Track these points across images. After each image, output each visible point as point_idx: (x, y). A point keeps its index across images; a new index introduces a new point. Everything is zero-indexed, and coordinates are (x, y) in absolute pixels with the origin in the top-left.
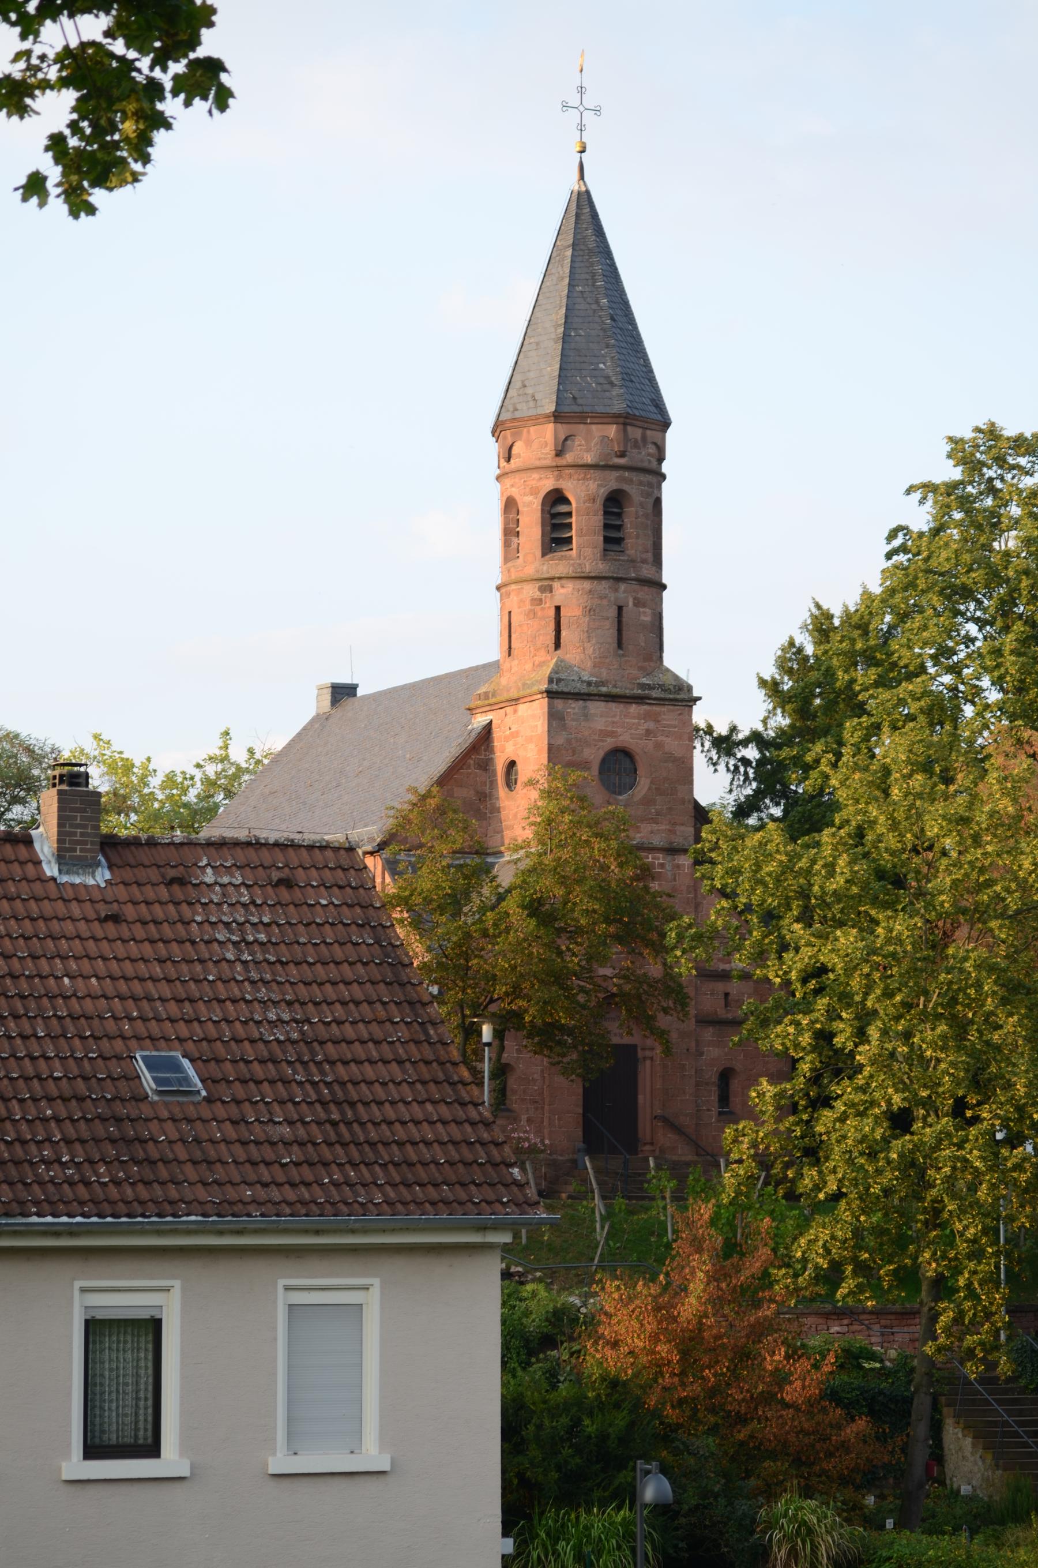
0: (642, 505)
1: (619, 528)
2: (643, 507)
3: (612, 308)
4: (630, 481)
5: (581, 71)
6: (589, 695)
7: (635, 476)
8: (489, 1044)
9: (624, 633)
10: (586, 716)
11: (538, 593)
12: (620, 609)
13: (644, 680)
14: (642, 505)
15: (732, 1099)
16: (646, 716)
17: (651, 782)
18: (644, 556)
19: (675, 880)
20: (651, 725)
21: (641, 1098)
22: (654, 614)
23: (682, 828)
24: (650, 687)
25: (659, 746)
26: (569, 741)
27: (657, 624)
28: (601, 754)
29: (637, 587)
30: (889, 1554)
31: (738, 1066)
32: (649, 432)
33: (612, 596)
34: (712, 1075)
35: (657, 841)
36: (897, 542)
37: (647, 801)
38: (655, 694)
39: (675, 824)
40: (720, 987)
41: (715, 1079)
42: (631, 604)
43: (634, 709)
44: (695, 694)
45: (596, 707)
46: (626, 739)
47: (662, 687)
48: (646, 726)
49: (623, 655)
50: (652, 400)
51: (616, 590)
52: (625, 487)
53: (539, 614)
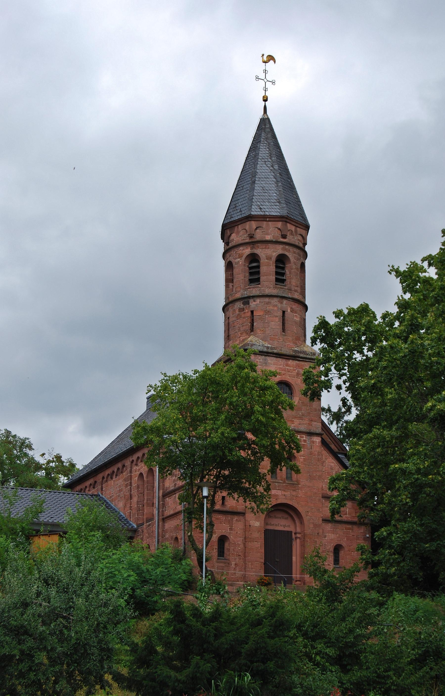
1: (283, 274)
2: (295, 265)
3: (280, 170)
6: (268, 353)
7: (291, 249)
8: (206, 497)
9: (286, 325)
11: (242, 305)
12: (284, 312)
15: (340, 561)
16: (298, 366)
17: (299, 399)
18: (296, 288)
19: (312, 449)
21: (294, 558)
22: (301, 318)
23: (315, 423)
24: (298, 352)
27: (303, 323)
29: (293, 303)
31: (344, 544)
32: (298, 229)
33: (279, 305)
35: (302, 428)
38: (302, 355)
39: (312, 420)
41: (332, 549)
42: (289, 311)
43: (290, 362)
45: (271, 360)
47: (304, 353)
49: (285, 335)
50: (300, 214)
51: (282, 303)
52: (287, 253)
53: (243, 316)
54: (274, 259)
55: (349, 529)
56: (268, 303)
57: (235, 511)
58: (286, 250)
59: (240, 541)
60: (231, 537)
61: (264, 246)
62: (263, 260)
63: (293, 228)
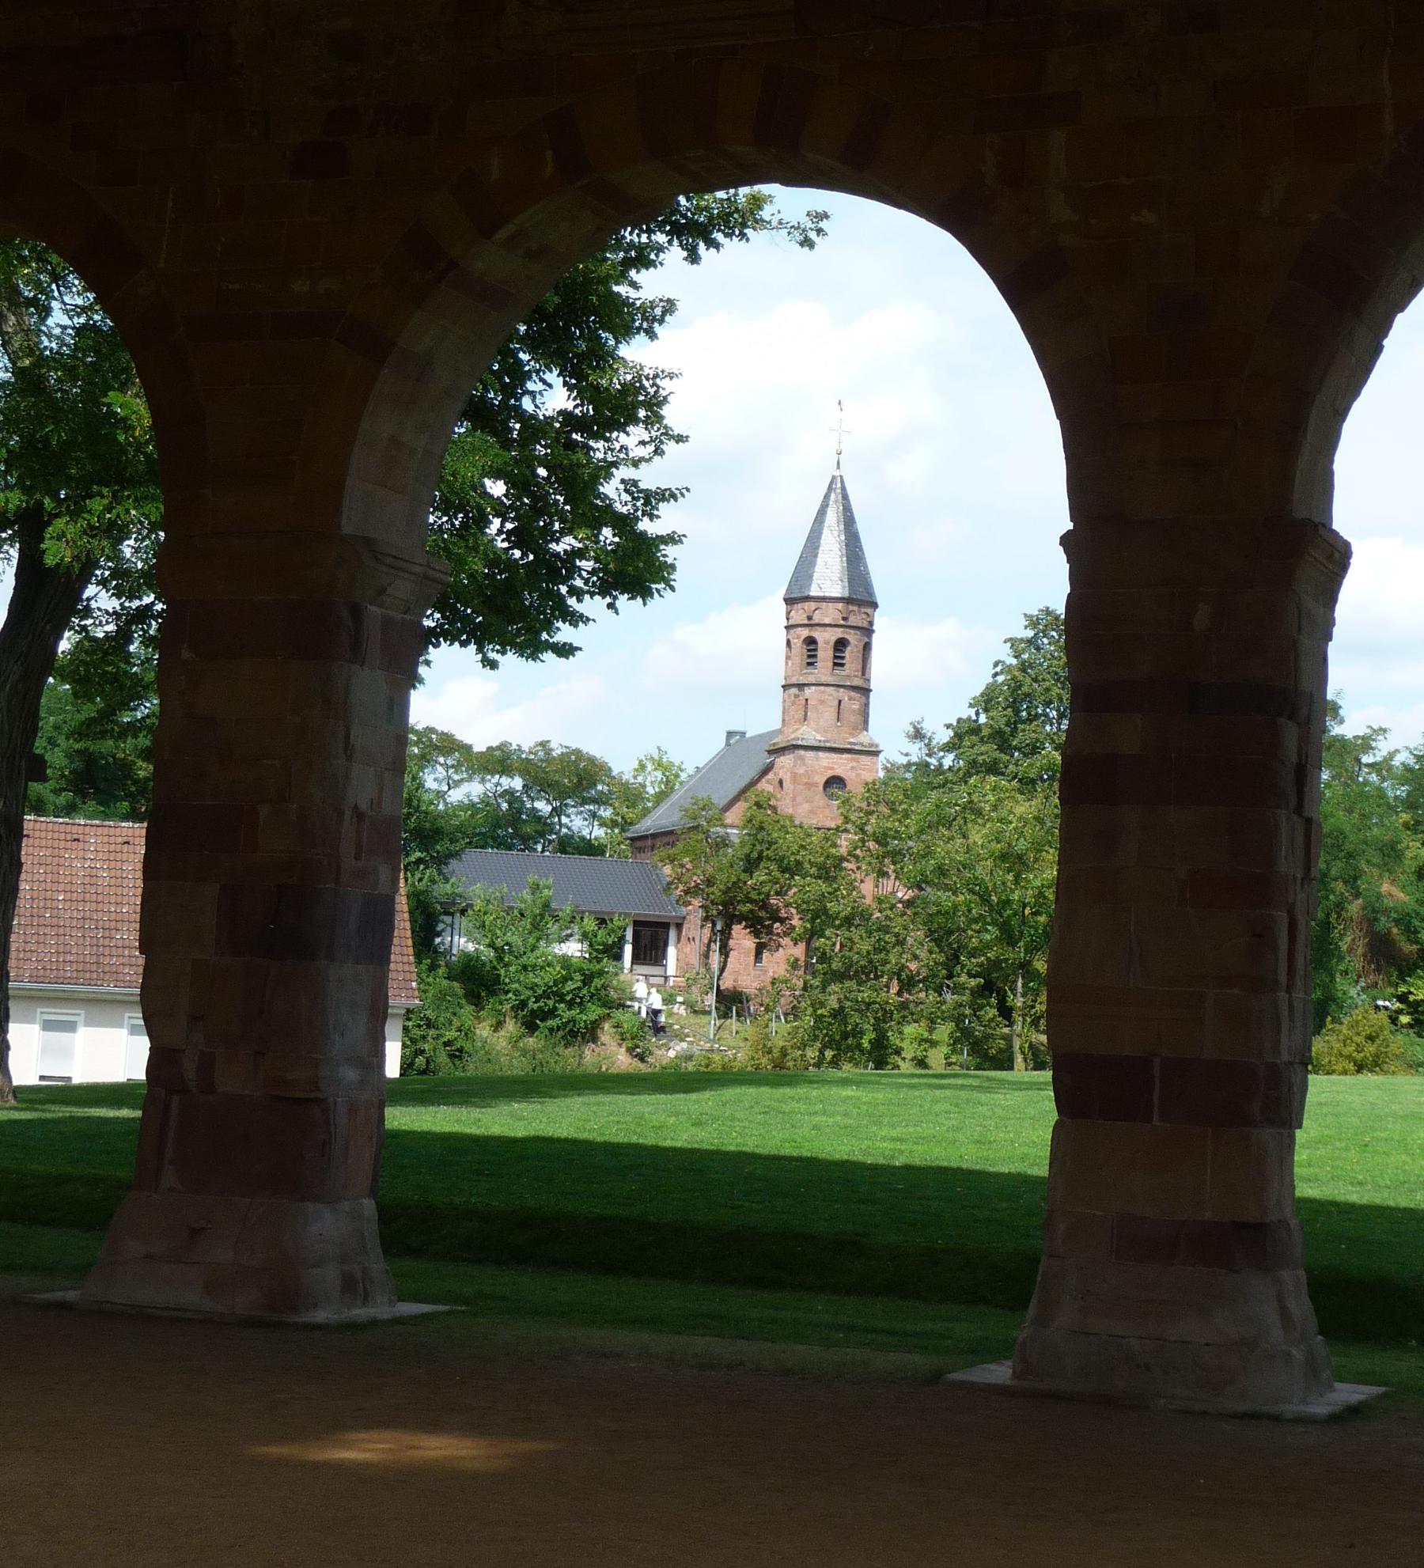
0: (856, 646)
10: (817, 759)
12: (840, 701)
13: (852, 740)
14: (856, 646)
16: (852, 760)
20: (854, 764)
24: (854, 744)
25: (858, 775)
26: (806, 771)
28: (825, 779)
30: (534, 953)
36: (998, 669)
38: (856, 748)
43: (845, 756)
44: (881, 748)
46: (839, 771)
48: (851, 765)
52: (847, 637)
56: (823, 692)
58: (847, 633)
62: (821, 644)
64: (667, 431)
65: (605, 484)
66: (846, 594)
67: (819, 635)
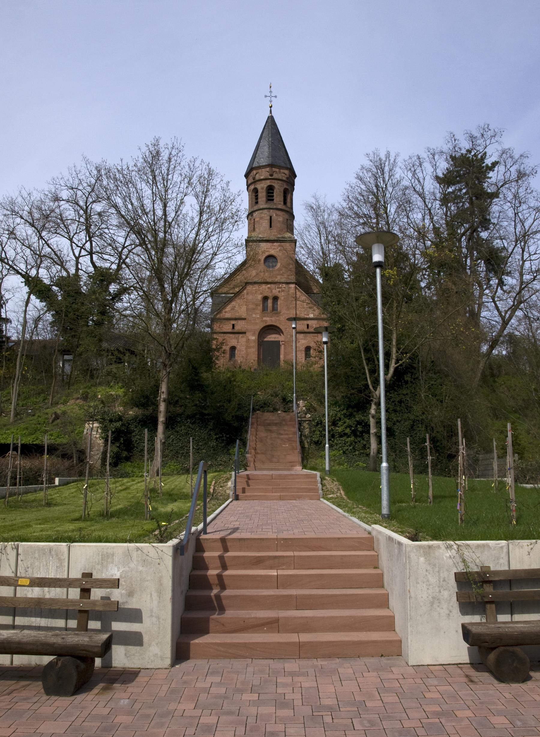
4: (275, 183)
5: (271, 87)
7: (276, 181)
12: (271, 217)
33: (268, 213)
34: (303, 348)
37: (279, 270)
40: (306, 322)
41: (304, 349)
45: (263, 245)
46: (272, 252)
51: (269, 212)
54: (265, 189)
55: (315, 336)
56: (261, 213)
57: (240, 331)
58: (272, 182)
59: (243, 348)
60: (238, 347)
61: (260, 182)
62: (260, 190)
63: (277, 170)
64: (172, 302)
65: (131, 164)
66: (270, 162)
67: (259, 186)
